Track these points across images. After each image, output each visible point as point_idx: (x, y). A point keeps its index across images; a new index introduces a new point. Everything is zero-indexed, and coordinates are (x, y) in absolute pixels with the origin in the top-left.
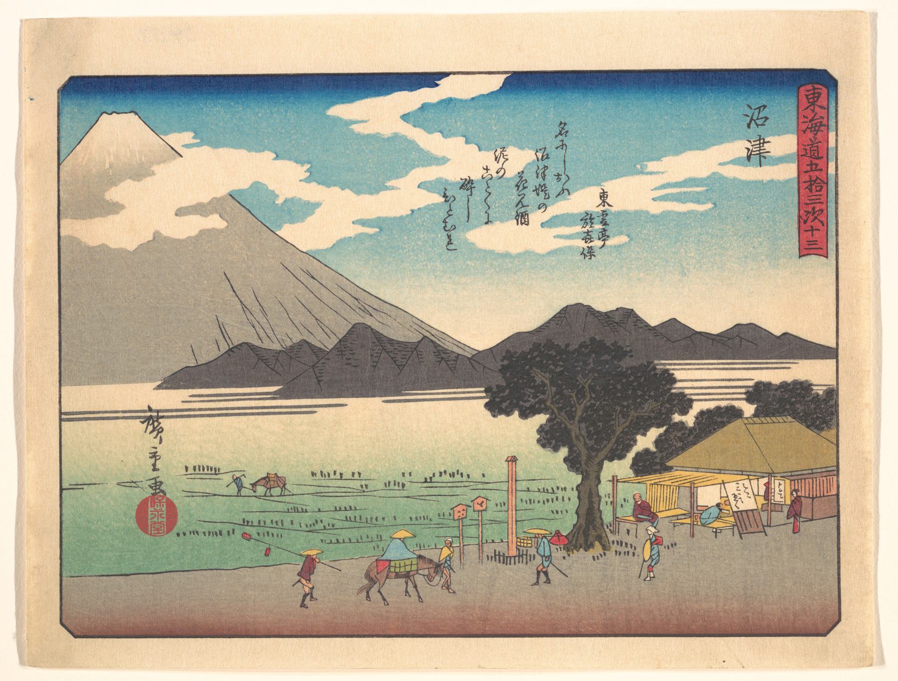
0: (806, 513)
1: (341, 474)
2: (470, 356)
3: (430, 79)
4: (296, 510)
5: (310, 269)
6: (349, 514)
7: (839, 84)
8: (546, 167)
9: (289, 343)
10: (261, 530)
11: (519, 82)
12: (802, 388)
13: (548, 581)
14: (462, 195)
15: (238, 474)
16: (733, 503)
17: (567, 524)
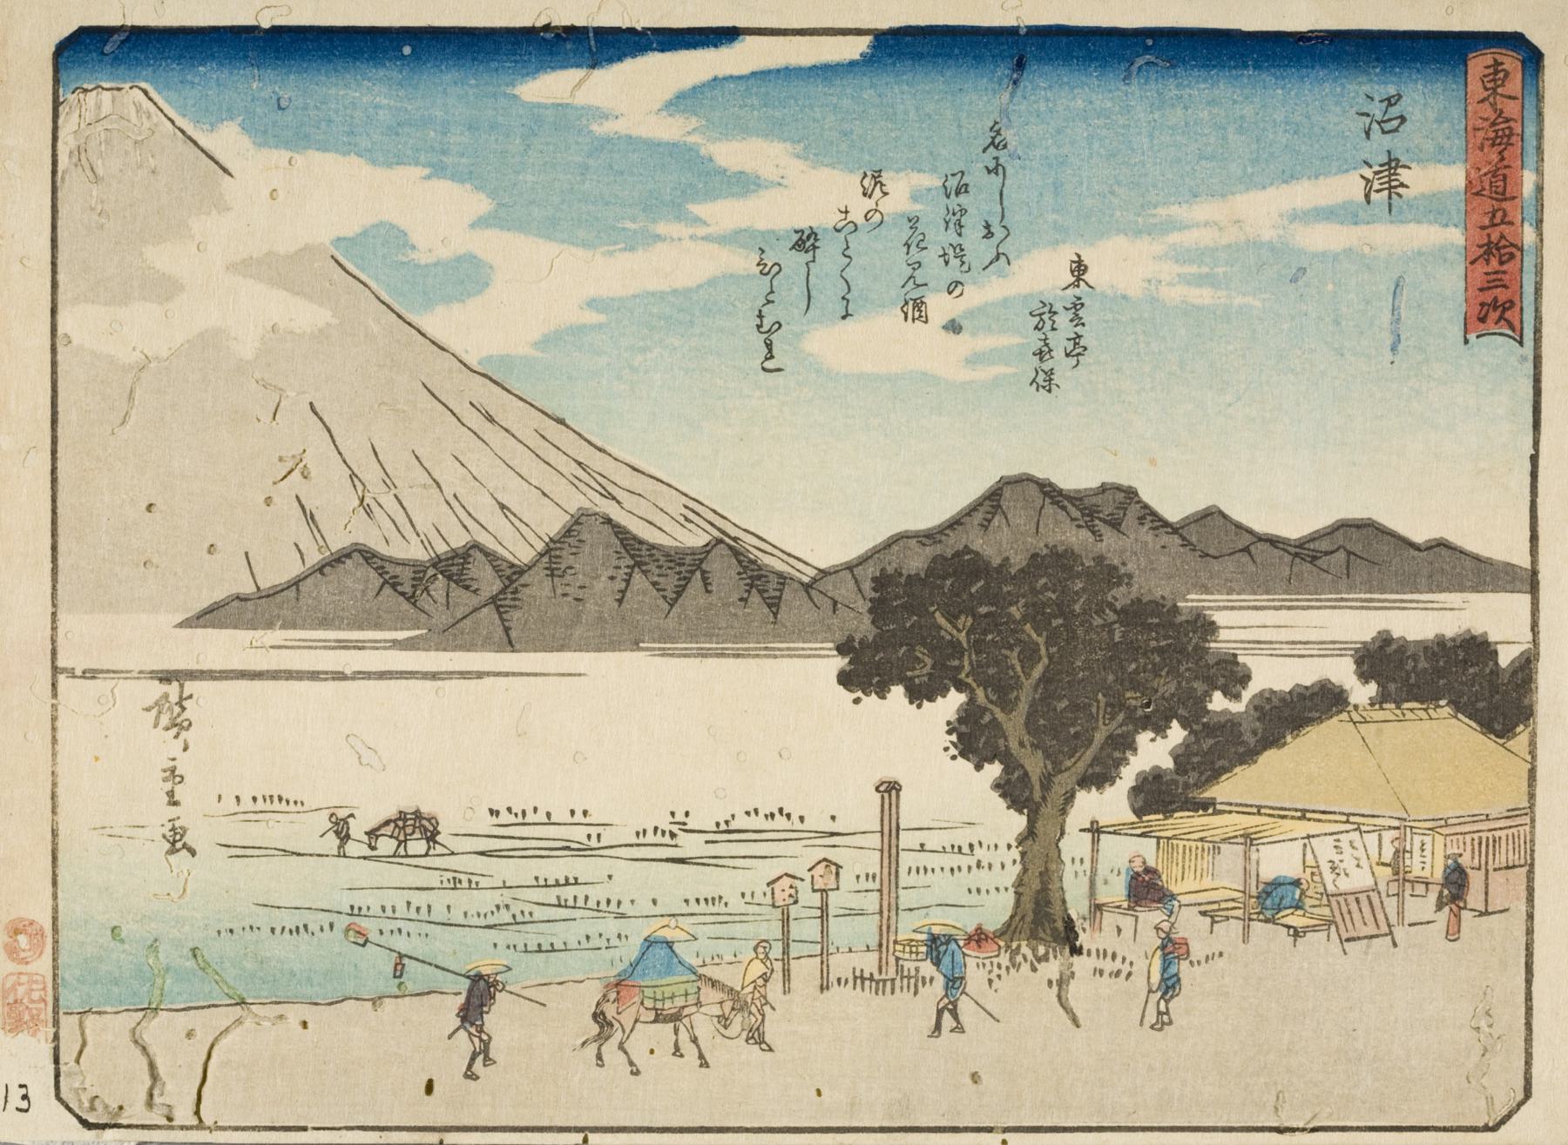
0: (1474, 898)
1: (548, 815)
2: (806, 580)
3: (725, 35)
4: (455, 884)
5: (494, 393)
6: (568, 893)
7: (1547, 62)
8: (964, 211)
9: (442, 548)
10: (388, 926)
11: (904, 46)
12: (1476, 648)
13: (959, 1028)
14: (794, 262)
15: (342, 814)
16: (1328, 877)
17: (997, 910)
